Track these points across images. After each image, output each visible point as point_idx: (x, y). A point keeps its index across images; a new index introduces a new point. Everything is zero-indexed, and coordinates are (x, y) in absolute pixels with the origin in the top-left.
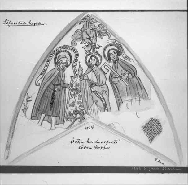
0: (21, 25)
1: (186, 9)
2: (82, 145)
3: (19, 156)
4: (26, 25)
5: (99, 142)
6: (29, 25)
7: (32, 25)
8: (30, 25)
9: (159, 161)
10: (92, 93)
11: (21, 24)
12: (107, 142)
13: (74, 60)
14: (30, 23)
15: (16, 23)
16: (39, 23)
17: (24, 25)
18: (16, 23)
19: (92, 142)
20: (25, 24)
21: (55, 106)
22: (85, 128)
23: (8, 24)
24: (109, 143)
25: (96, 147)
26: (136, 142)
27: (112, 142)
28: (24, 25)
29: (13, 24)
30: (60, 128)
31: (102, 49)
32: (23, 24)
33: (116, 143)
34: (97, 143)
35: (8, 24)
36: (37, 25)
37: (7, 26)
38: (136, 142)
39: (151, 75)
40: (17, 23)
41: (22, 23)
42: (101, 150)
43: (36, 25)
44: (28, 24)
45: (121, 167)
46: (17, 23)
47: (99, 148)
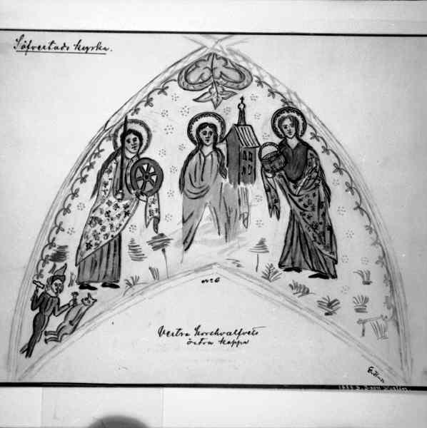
0: (57, 51)
1: (425, 32)
2: (169, 173)
4: (69, 51)
6: (74, 51)
7: (82, 51)
8: (77, 51)
9: (376, 374)
12: (239, 334)
16: (98, 47)
17: (63, 51)
19: (206, 334)
21: (162, 288)
22: (203, 282)
23: (25, 49)
24: (244, 334)
25: (222, 341)
27: (249, 333)
28: (63, 51)
29: (36, 50)
30: (78, 244)
31: (254, 80)
32: (62, 48)
33: (257, 333)
35: (27, 48)
36: (92, 52)
37: (24, 53)
43: (89, 51)
44: (72, 49)
46: (44, 47)
47: (229, 343)
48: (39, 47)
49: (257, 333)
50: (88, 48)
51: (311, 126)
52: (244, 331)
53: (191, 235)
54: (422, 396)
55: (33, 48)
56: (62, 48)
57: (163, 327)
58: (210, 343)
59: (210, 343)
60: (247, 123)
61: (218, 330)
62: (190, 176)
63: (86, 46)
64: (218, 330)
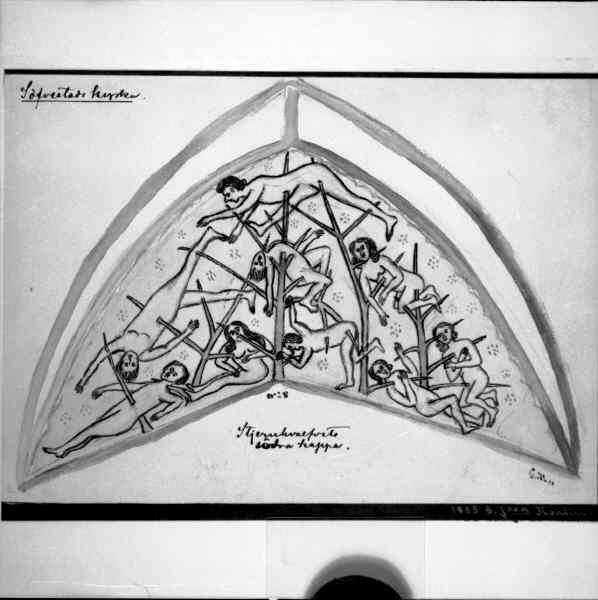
5: (291, 434)
6: (91, 99)
8: (96, 98)
11: (71, 96)
16: (122, 93)
29: (49, 98)
30: (159, 294)
32: (77, 96)
42: (316, 451)
43: (114, 98)
44: (88, 97)
46: (59, 95)
48: (53, 95)
49: (336, 435)
50: (111, 95)
51: (561, 467)
52: (313, 449)
53: (216, 217)
54: (595, 81)
55: (45, 96)
56: (77, 96)
57: (96, 87)
58: (336, 446)
59: (289, 446)
60: (419, 272)
61: (285, 429)
62: (309, 440)
63: (108, 92)
64: (285, 429)
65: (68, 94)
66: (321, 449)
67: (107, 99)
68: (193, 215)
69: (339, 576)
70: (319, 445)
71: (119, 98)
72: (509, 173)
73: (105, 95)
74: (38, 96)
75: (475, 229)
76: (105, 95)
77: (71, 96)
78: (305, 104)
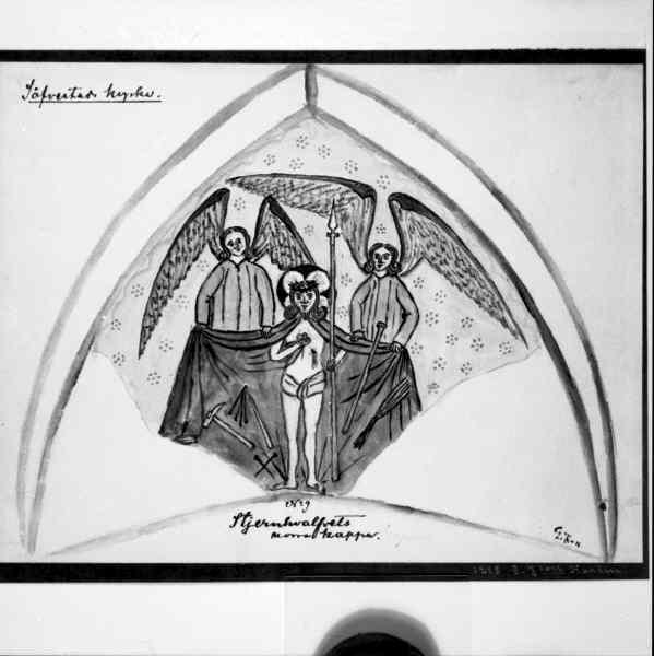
3: (29, 397)
5: (296, 524)
7: (118, 99)
10: (279, 340)
13: (569, 553)
14: (110, 93)
15: (62, 95)
16: (139, 92)
18: (62, 95)
20: (92, 98)
26: (261, 88)
32: (88, 96)
34: (291, 524)
38: (261, 88)
39: (604, 428)
40: (65, 96)
41: (84, 95)
43: (128, 99)
44: (102, 96)
45: (510, 51)
46: (65, 96)
48: (58, 96)
54: (638, 591)
56: (88, 96)
57: (111, 85)
65: (76, 94)
66: (352, 539)
67: (122, 98)
68: (510, 295)
69: (365, 629)
70: (358, 534)
71: (134, 98)
72: (552, 174)
73: (119, 94)
74: (44, 97)
75: (587, 366)
76: (119, 94)
77: (80, 96)
78: (324, 84)
